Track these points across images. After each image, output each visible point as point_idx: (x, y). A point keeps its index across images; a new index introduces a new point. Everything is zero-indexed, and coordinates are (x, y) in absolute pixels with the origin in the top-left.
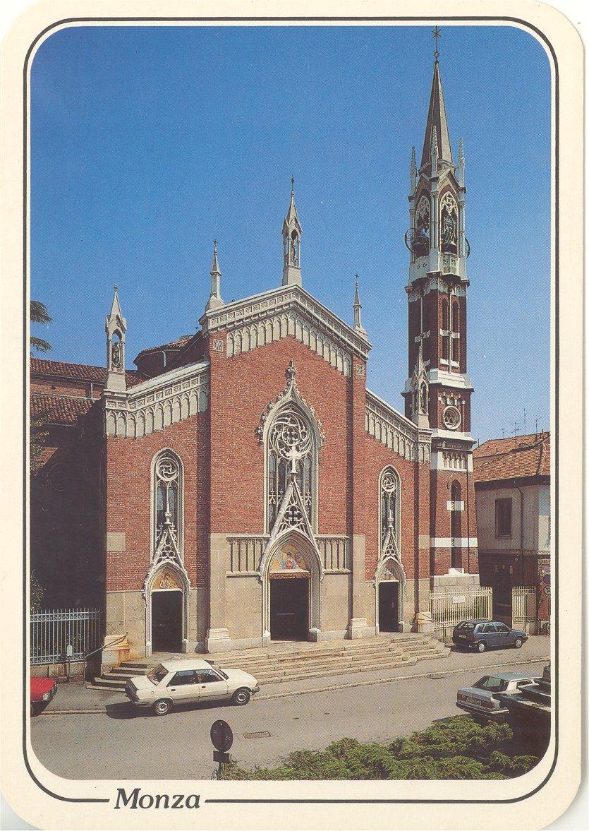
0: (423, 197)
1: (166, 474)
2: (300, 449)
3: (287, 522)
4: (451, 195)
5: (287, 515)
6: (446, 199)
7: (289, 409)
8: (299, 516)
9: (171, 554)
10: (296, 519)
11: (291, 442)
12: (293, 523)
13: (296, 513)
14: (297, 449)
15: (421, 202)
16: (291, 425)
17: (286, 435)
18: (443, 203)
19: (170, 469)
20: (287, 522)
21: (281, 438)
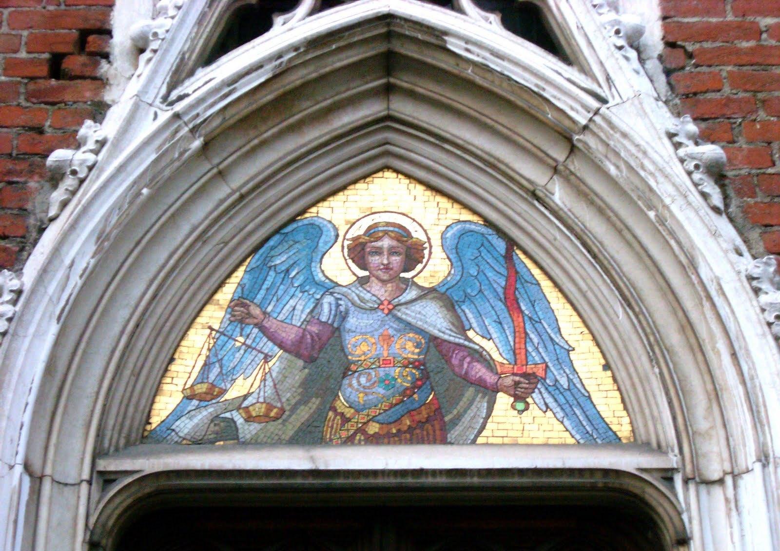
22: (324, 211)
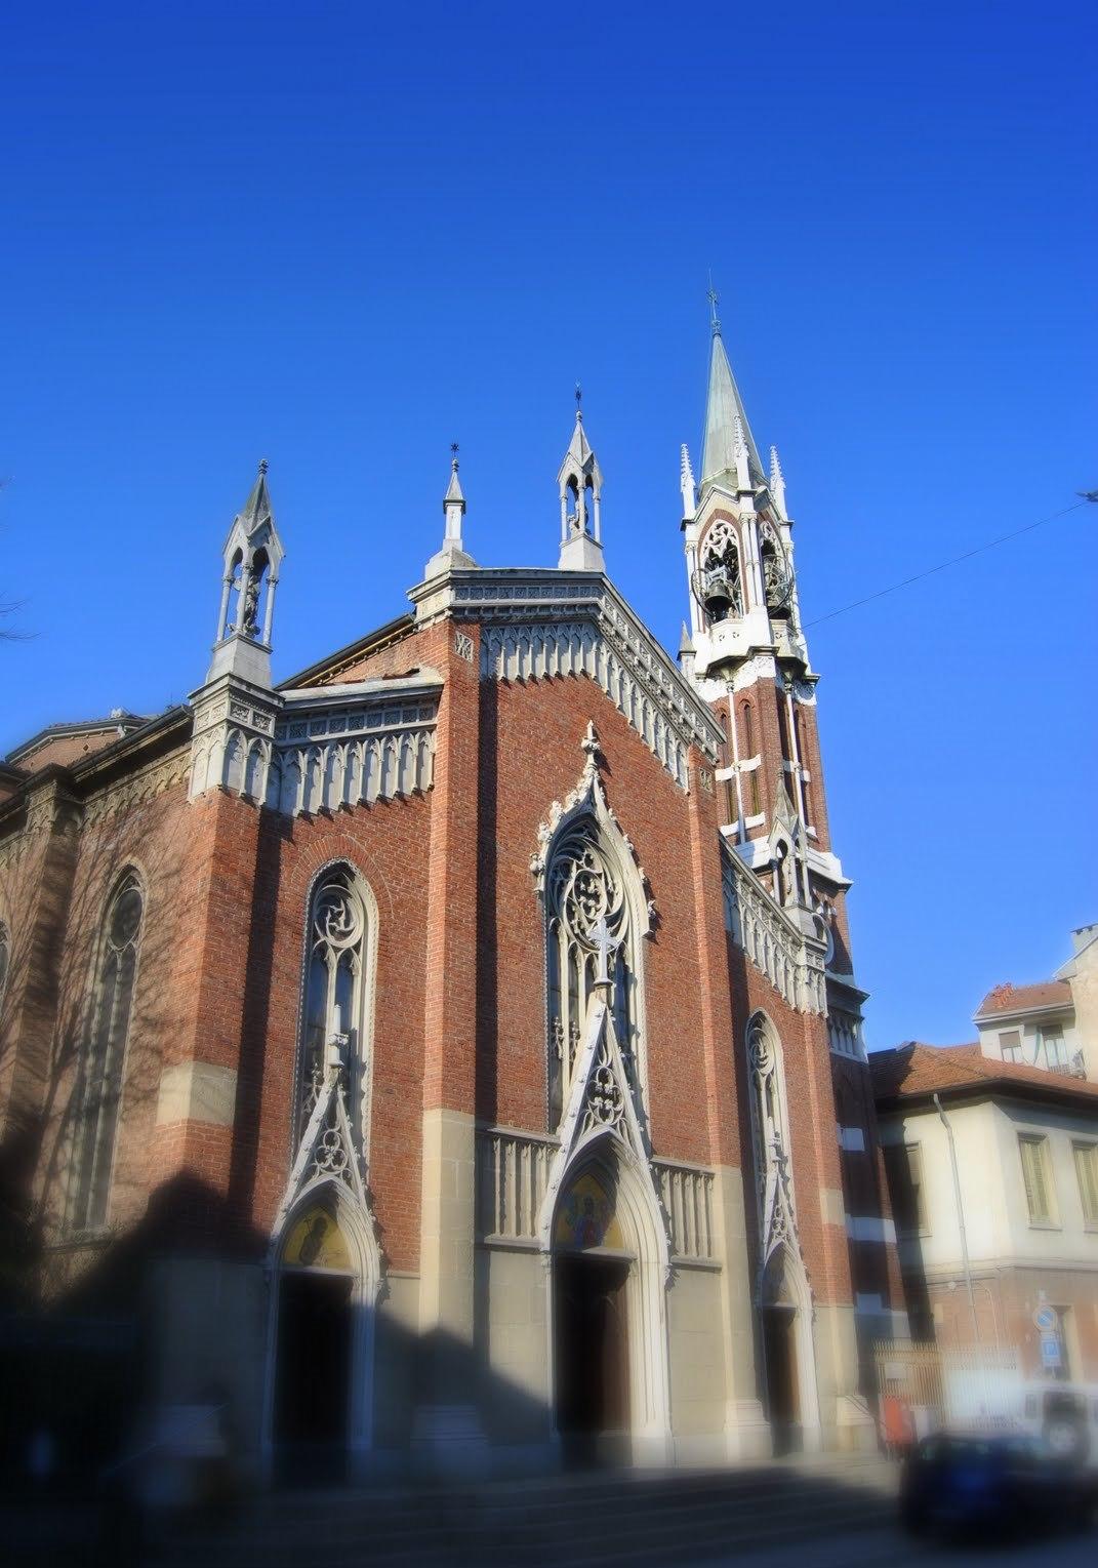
1: (347, 924)
7: (582, 831)
19: (329, 915)
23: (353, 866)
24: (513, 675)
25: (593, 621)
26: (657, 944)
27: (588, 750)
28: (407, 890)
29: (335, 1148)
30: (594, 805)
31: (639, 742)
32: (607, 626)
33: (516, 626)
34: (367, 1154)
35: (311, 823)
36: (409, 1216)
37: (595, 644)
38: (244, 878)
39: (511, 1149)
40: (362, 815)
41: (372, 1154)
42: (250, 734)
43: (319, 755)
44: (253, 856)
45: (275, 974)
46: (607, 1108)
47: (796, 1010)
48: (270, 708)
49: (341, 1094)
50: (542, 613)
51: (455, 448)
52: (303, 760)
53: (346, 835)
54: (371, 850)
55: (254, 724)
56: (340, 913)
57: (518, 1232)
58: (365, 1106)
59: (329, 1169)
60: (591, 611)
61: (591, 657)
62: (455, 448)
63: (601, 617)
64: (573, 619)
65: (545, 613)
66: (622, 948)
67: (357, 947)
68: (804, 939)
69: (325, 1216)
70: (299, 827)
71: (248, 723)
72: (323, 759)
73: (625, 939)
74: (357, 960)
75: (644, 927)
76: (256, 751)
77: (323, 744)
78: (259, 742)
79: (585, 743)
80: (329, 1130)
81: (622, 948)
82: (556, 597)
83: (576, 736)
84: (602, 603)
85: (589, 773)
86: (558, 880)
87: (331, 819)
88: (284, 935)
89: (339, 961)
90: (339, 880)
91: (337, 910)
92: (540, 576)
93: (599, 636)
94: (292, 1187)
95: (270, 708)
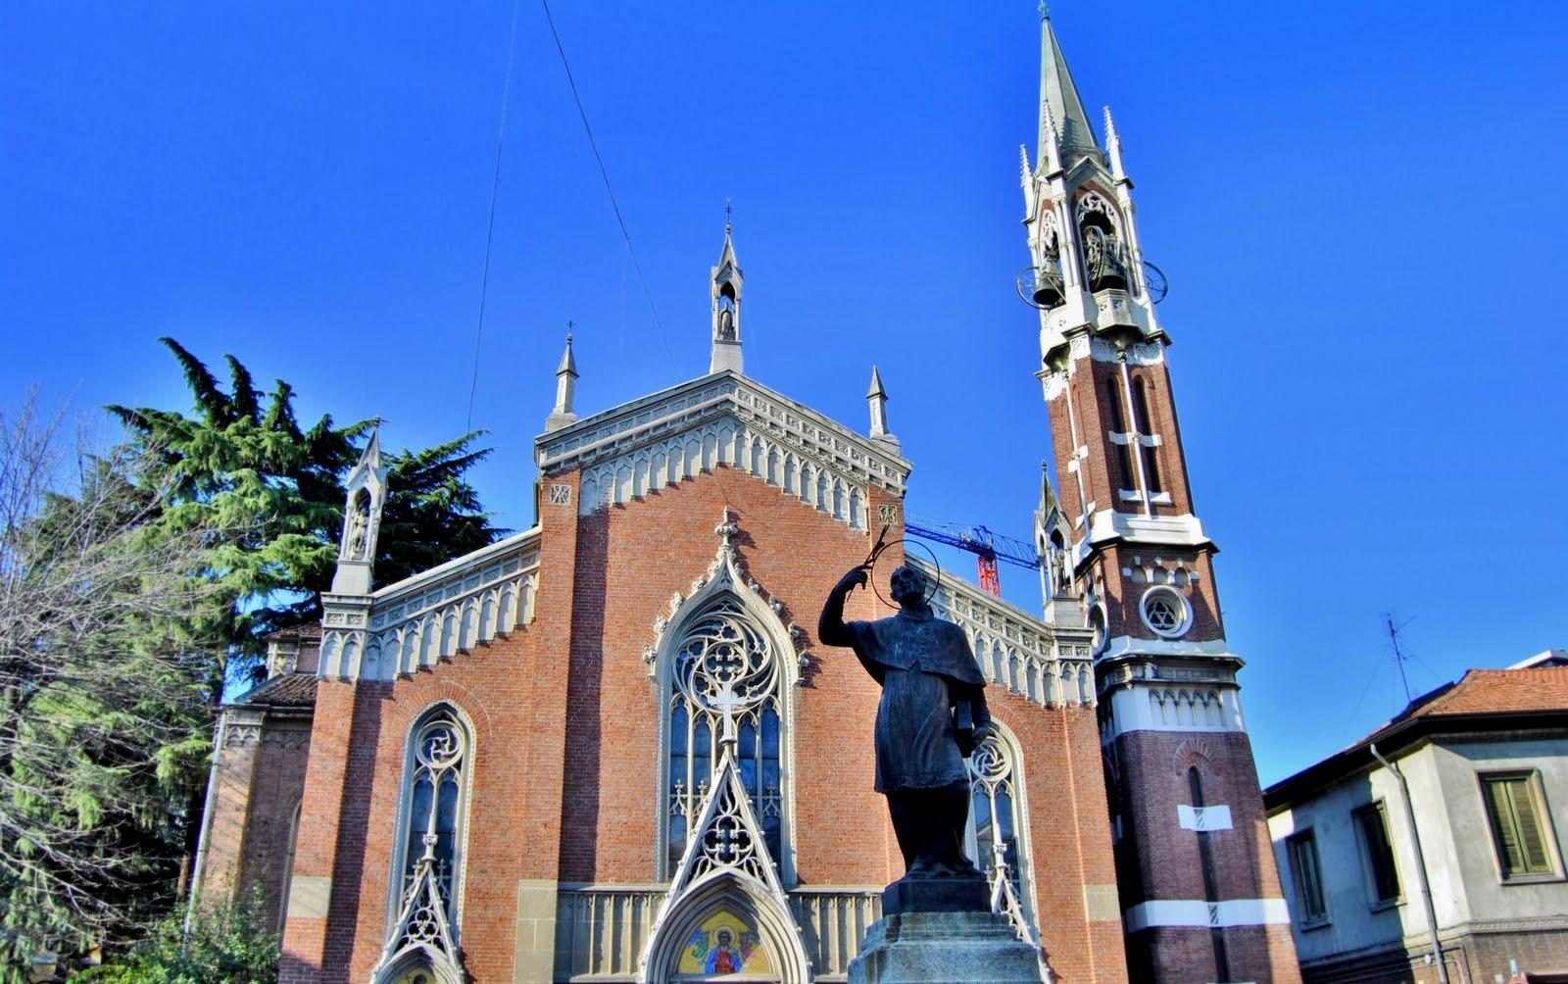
0: (1046, 211)
1: (452, 747)
2: (748, 690)
3: (712, 856)
4: (1097, 194)
5: (711, 839)
6: (1086, 204)
7: (720, 607)
8: (744, 840)
9: (430, 930)
10: (734, 848)
11: (725, 676)
12: (727, 857)
13: (734, 833)
14: (739, 690)
15: (1044, 223)
16: (728, 640)
17: (711, 662)
18: (1080, 211)
19: (434, 745)
20: (712, 856)
21: (700, 669)
22: (705, 928)
23: (451, 703)
24: (626, 497)
25: (728, 414)
26: (815, 688)
27: (721, 534)
28: (507, 708)
29: (426, 923)
30: (730, 581)
31: (797, 505)
32: (743, 415)
33: (630, 453)
34: (1037, 925)
35: (411, 680)
36: (502, 967)
37: (735, 435)
38: (340, 739)
39: (833, 904)
40: (461, 662)
41: (464, 922)
42: (1075, 662)
43: (416, 626)
44: (348, 721)
45: (373, 800)
46: (732, 851)
47: (1049, 707)
48: (361, 607)
49: (1008, 886)
50: (657, 433)
51: (571, 324)
52: (401, 636)
53: (446, 680)
54: (470, 687)
55: (349, 623)
56: (445, 742)
57: (616, 967)
58: (1032, 891)
59: (421, 938)
60: (725, 407)
61: (731, 449)
62: (571, 324)
63: (736, 409)
64: (702, 422)
65: (662, 431)
66: (769, 702)
67: (1009, 778)
68: (1053, 633)
69: (426, 974)
70: (399, 687)
71: (1074, 656)
72: (420, 630)
73: (775, 692)
74: (1011, 787)
75: (793, 676)
76: (1082, 672)
77: (419, 618)
78: (353, 635)
79: (719, 528)
80: (421, 909)
81: (769, 702)
82: (674, 411)
83: (706, 526)
84: (734, 397)
85: (723, 553)
86: (686, 660)
87: (430, 672)
88: (382, 771)
89: (996, 791)
90: (444, 716)
91: (441, 739)
92: (646, 403)
93: (740, 425)
94: (385, 954)
95: (361, 607)
